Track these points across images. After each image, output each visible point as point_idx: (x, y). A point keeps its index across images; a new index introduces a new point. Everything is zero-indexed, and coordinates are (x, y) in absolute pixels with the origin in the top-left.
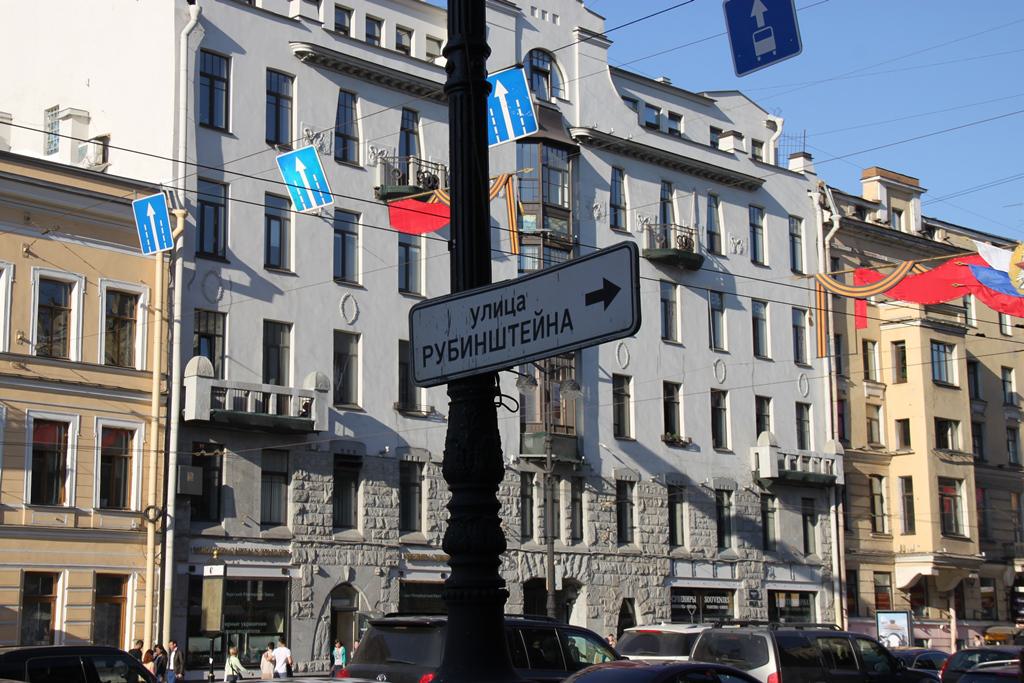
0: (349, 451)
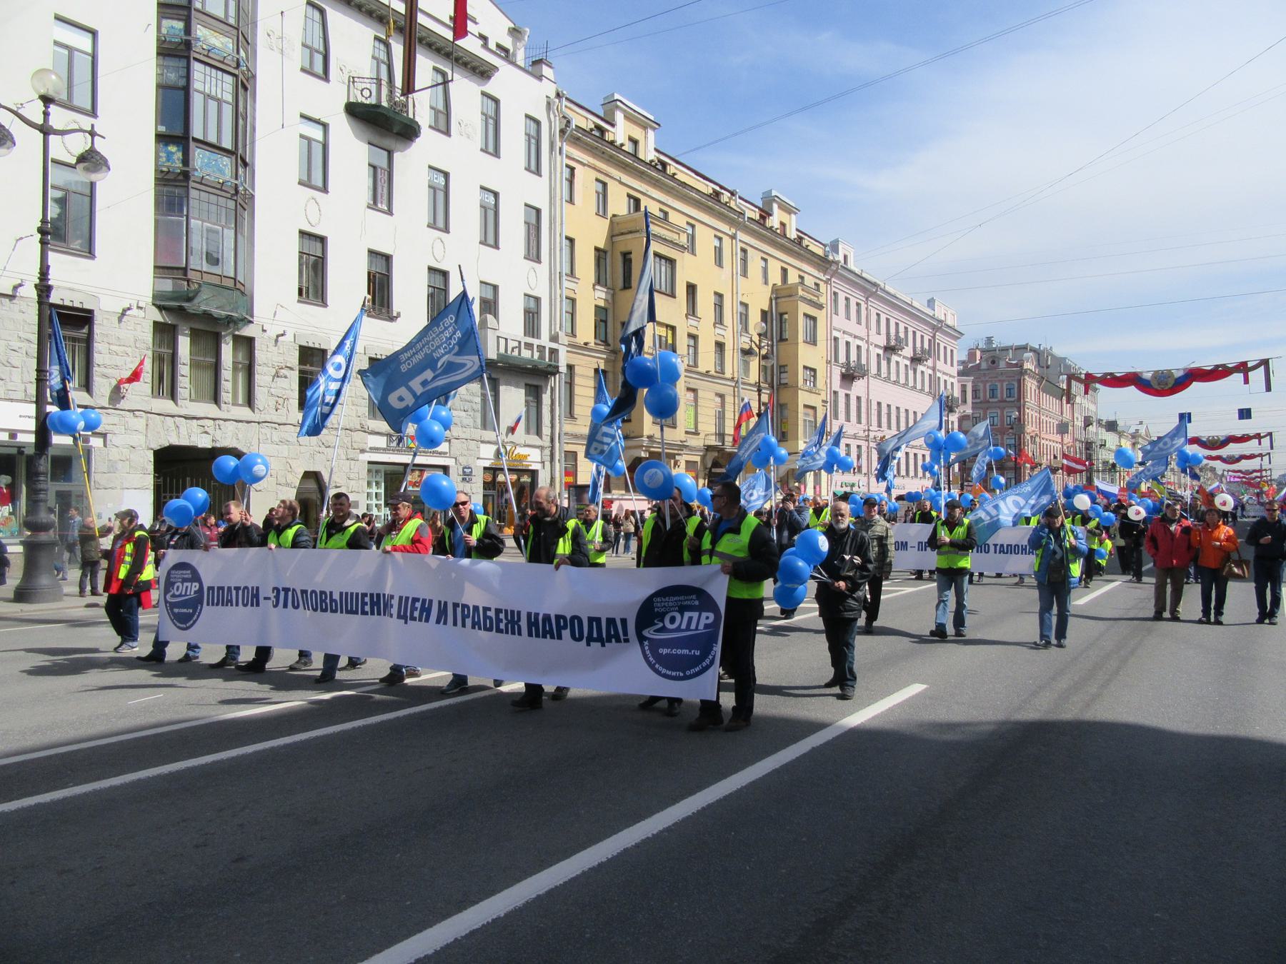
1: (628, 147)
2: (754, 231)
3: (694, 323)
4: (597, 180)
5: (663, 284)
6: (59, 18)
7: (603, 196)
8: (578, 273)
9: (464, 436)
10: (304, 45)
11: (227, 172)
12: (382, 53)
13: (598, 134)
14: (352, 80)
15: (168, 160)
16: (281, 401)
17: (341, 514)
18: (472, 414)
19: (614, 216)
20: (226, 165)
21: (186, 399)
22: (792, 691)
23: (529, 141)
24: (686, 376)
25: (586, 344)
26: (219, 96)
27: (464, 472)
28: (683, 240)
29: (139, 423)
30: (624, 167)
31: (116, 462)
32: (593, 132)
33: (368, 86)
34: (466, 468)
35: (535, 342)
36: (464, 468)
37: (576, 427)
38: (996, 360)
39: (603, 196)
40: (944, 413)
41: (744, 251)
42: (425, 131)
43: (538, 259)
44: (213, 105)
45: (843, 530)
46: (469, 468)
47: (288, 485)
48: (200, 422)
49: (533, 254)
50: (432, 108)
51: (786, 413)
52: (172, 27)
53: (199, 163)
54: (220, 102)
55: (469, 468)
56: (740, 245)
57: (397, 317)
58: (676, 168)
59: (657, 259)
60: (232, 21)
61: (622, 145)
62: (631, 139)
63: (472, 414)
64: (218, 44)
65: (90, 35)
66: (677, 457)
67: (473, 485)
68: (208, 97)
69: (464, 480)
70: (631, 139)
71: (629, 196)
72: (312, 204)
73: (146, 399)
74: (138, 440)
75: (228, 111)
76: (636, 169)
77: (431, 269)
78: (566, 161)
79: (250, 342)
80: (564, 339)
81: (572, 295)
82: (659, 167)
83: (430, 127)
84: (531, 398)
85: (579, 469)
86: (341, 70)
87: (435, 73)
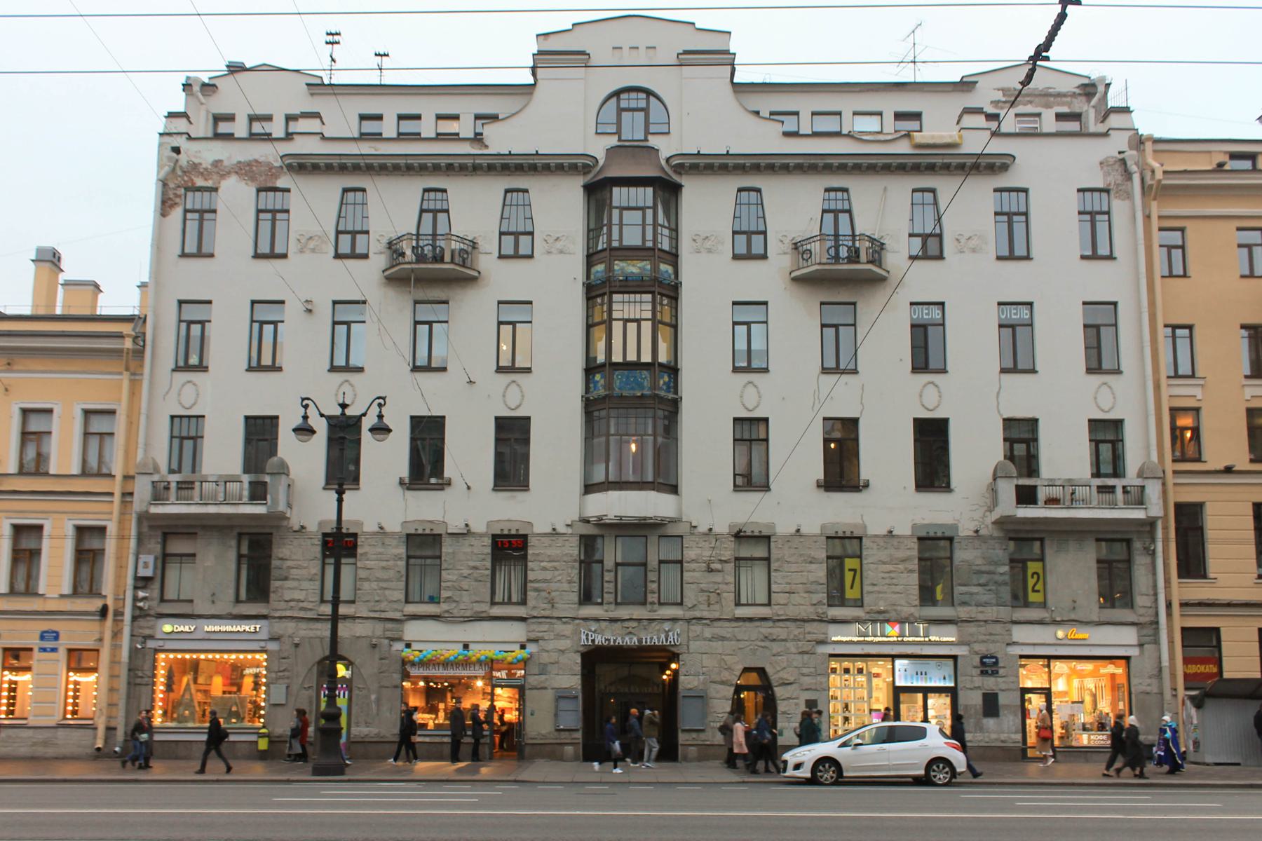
0: (935, 533)
6: (364, 322)
9: (981, 617)
11: (646, 384)
18: (993, 588)
21: (611, 603)
22: (462, 619)
24: (1175, 472)
27: (983, 664)
29: (567, 629)
31: (545, 665)
32: (1227, 167)
34: (986, 657)
35: (1117, 483)
36: (982, 658)
38: (8, 388)
44: (632, 327)
46: (992, 657)
47: (723, 683)
48: (626, 624)
51: (1095, 471)
53: (618, 384)
55: (992, 657)
63: (993, 588)
64: (635, 270)
67: (1000, 680)
69: (983, 673)
72: (1105, 389)
73: (573, 606)
74: (564, 644)
85: (1224, 653)
86: (782, 241)
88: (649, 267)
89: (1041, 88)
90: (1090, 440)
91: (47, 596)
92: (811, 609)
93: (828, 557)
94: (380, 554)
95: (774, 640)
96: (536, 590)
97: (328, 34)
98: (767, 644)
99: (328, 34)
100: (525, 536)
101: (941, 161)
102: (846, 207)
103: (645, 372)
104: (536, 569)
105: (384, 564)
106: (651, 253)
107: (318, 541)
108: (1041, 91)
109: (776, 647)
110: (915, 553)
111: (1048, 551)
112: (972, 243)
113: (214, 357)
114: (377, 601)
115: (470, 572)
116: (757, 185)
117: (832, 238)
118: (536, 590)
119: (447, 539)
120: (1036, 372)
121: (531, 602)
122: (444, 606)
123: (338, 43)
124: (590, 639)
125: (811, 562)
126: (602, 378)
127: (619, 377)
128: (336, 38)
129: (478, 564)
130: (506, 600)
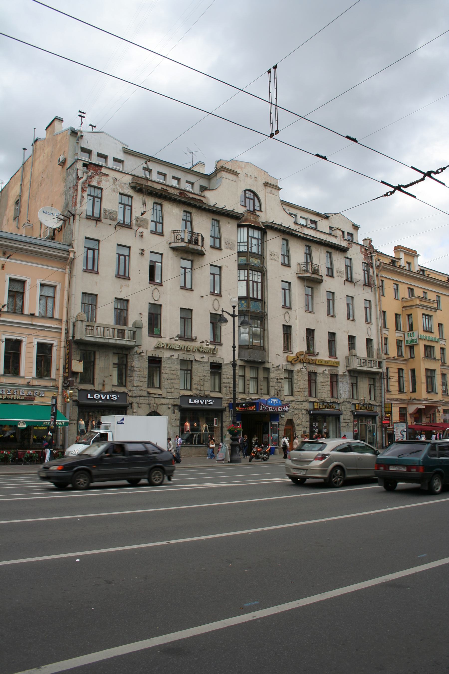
1: (407, 268)
2: (391, 270)
3: (443, 343)
4: (394, 284)
5: (255, 293)
7: (396, 290)
8: (387, 326)
10: (282, 255)
12: (308, 251)
13: (421, 273)
14: (299, 264)
15: (242, 307)
16: (279, 391)
17: (37, 455)
19: (403, 298)
20: (260, 305)
23: (365, 273)
25: (394, 357)
26: (257, 281)
28: (435, 305)
30: (407, 276)
33: (180, 234)
37: (391, 395)
39: (396, 290)
40: (262, 345)
41: (382, 281)
42: (325, 278)
43: (371, 323)
44: (255, 284)
45: (292, 480)
49: (368, 321)
50: (326, 267)
52: (242, 260)
54: (257, 283)
56: (380, 279)
57: (317, 355)
58: (429, 272)
59: (424, 316)
60: (260, 253)
61: (404, 267)
62: (407, 263)
65: (128, 249)
66: (439, 408)
68: (254, 282)
70: (407, 263)
71: (409, 288)
75: (259, 285)
76: (403, 274)
77: (329, 332)
78: (380, 279)
79: (268, 369)
80: (384, 356)
81: (386, 336)
82: (421, 273)
83: (327, 275)
84: (6, 370)
87: (283, 240)
88: (260, 262)
89: (75, 129)
90: (181, 318)
91: (26, 377)
92: (304, 398)
93: (181, 370)
94: (171, 367)
95: (295, 409)
96: (226, 387)
97: (80, 112)
98: (293, 410)
99: (80, 112)
100: (161, 358)
101: (184, 200)
102: (100, 196)
103: (259, 303)
104: (207, 376)
105: (172, 372)
106: (246, 254)
107: (146, 359)
108: (75, 130)
109: (296, 412)
110: (147, 366)
111: (359, 380)
112: (275, 257)
113: (133, 274)
114: (170, 388)
115: (203, 377)
116: (191, 211)
117: (305, 264)
118: (226, 387)
119: (195, 363)
120: (193, 290)
121: (296, 393)
122: (195, 392)
123: (84, 117)
124: (263, 408)
125: (304, 381)
126: (245, 303)
127: (252, 304)
128: (83, 115)
129: (205, 374)
130: (186, 389)
